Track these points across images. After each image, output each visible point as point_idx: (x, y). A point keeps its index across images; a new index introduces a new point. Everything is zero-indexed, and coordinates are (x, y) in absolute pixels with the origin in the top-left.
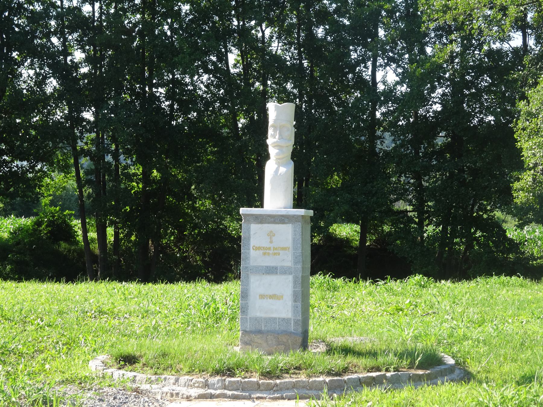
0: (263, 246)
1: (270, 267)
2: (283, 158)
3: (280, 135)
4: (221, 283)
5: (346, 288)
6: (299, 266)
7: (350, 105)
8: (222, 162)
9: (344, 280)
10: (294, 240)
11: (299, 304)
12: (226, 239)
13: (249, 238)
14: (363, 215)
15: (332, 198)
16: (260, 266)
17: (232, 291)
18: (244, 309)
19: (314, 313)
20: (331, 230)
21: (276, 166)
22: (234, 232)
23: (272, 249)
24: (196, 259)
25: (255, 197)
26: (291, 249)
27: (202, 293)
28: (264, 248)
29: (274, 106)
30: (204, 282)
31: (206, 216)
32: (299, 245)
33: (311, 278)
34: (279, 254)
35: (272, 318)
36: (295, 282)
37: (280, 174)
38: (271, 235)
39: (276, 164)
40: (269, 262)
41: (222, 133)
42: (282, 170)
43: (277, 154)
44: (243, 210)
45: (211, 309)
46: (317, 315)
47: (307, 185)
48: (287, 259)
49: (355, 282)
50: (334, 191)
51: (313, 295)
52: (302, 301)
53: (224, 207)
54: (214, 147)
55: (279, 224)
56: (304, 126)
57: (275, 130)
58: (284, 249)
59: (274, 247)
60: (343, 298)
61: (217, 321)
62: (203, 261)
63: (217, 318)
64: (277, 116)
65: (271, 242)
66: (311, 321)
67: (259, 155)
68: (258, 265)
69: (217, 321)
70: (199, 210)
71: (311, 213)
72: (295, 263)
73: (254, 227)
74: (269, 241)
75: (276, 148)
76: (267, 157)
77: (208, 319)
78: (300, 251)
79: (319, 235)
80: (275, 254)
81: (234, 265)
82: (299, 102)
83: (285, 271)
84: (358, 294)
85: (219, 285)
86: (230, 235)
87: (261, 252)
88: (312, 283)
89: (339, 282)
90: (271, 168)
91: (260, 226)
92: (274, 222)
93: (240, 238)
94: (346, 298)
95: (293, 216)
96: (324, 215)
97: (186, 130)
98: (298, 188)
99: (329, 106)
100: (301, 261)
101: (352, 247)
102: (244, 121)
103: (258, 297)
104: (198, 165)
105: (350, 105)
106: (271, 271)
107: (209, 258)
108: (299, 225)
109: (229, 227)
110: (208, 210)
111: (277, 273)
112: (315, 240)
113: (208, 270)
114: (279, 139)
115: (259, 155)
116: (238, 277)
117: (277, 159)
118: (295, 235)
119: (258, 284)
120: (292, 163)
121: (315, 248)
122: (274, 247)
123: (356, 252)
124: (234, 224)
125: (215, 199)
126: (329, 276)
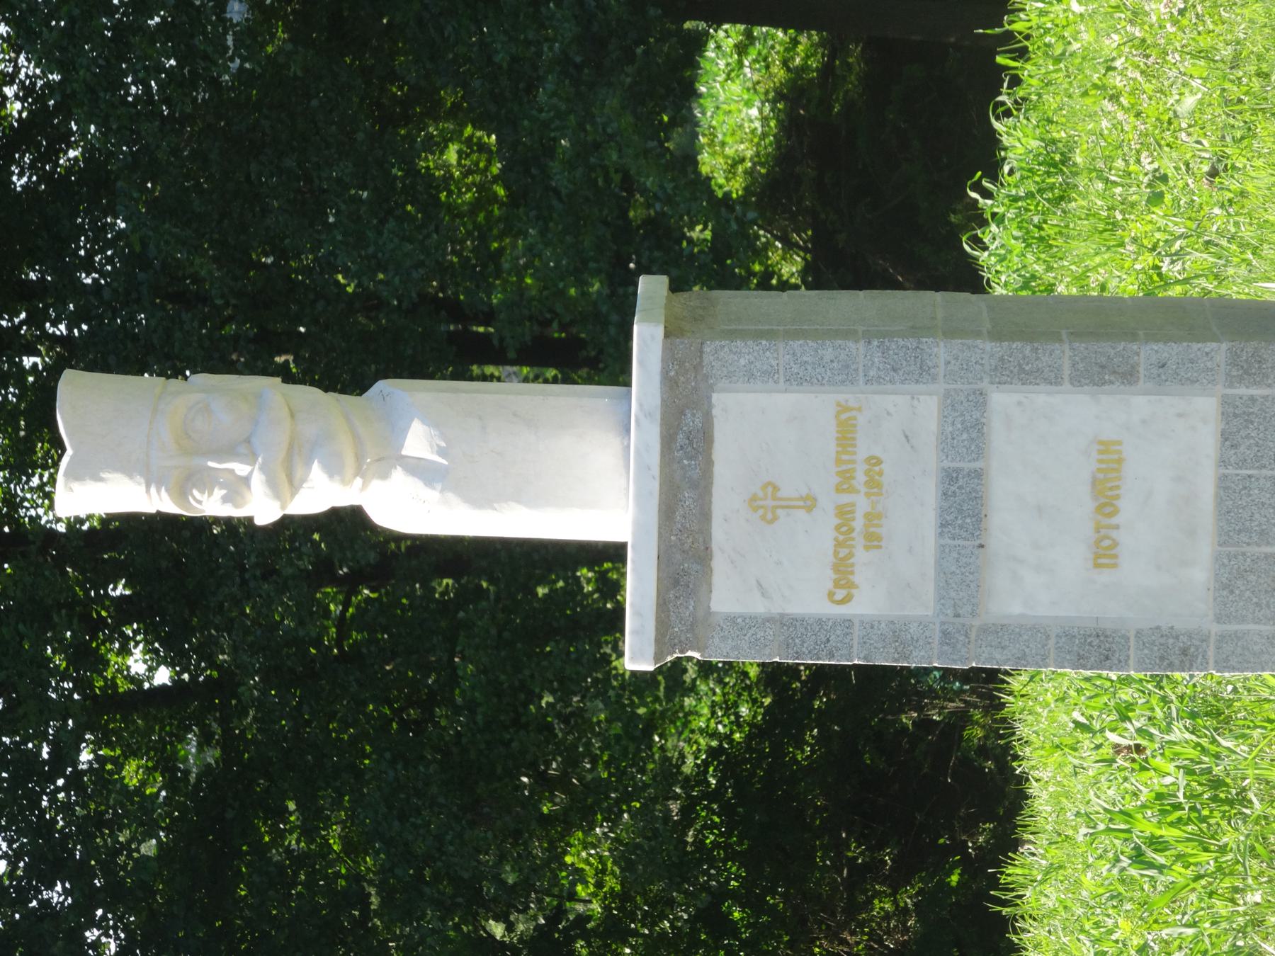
0: (829, 545)
1: (942, 511)
2: (356, 438)
3: (229, 451)
4: (1023, 779)
5: (1051, 102)
6: (940, 352)
7: (56, 77)
8: (358, 774)
9: (1008, 113)
10: (798, 380)
11: (1147, 353)
12: (778, 751)
13: (787, 623)
14: (653, 12)
15: (560, 178)
16: (939, 563)
17: (1064, 718)
18: (1172, 651)
19: (1190, 277)
20: (736, 187)
21: (398, 474)
22: (744, 710)
23: (845, 499)
24: (887, 917)
25: (554, 593)
26: (847, 396)
27: (1078, 882)
28: (838, 544)
29: (76, 486)
30: (1013, 872)
31: (655, 862)
32: (828, 353)
33: (999, 291)
34: (874, 461)
35: (1219, 501)
36: (1027, 376)
37: (441, 452)
38: (768, 504)
39: (385, 476)
40: (915, 516)
41: (206, 771)
42: (418, 441)
43: (333, 470)
44: (637, 656)
45: (1170, 833)
46: (1199, 259)
47: (488, 317)
48: (904, 419)
49: (1022, 54)
50: (525, 165)
51: (1094, 280)
52: (1133, 337)
53: (607, 765)
54: (283, 813)
55: (709, 463)
56: (160, 336)
57: (207, 481)
58: (846, 438)
59: (839, 489)
60: (1110, 117)
61: (1231, 803)
62: (896, 883)
63: (1215, 799)
64: (128, 470)
65: (809, 503)
66: (1237, 292)
67: (323, 572)
68: (931, 573)
69: (1231, 803)
70: (624, 897)
71: (651, 288)
72: (924, 373)
73: (728, 595)
74: (801, 514)
75: (299, 473)
76: (348, 523)
77: (1223, 849)
78: (858, 348)
79: (761, 253)
80: (874, 484)
81: (919, 709)
82: (37, 353)
83: (967, 432)
84: (1087, 37)
85: (1034, 788)
86: (757, 732)
87: (861, 556)
88: (1026, 286)
89: (1018, 140)
90: (407, 507)
91: (720, 565)
92: (703, 485)
93: (775, 676)
94: (1108, 105)
95: (670, 382)
96: (649, 222)
97: (524, 786)
98: (500, 360)
99: (60, 187)
100: (911, 343)
101: (827, 70)
102: (138, 652)
103: (1105, 577)
104: (375, 901)
105: (56, 77)
106: (964, 505)
107: (881, 847)
108: (717, 353)
109: (714, 735)
110: (627, 857)
111: (978, 475)
112: (790, 268)
113: (947, 851)
114: (250, 458)
115: (323, 572)
116: (987, 683)
117: (359, 472)
118: (770, 374)
119: (1037, 576)
120: (382, 386)
121: (833, 269)
122: (839, 489)
123: (855, 50)
124: (702, 708)
125: (566, 811)
126: (987, 194)
